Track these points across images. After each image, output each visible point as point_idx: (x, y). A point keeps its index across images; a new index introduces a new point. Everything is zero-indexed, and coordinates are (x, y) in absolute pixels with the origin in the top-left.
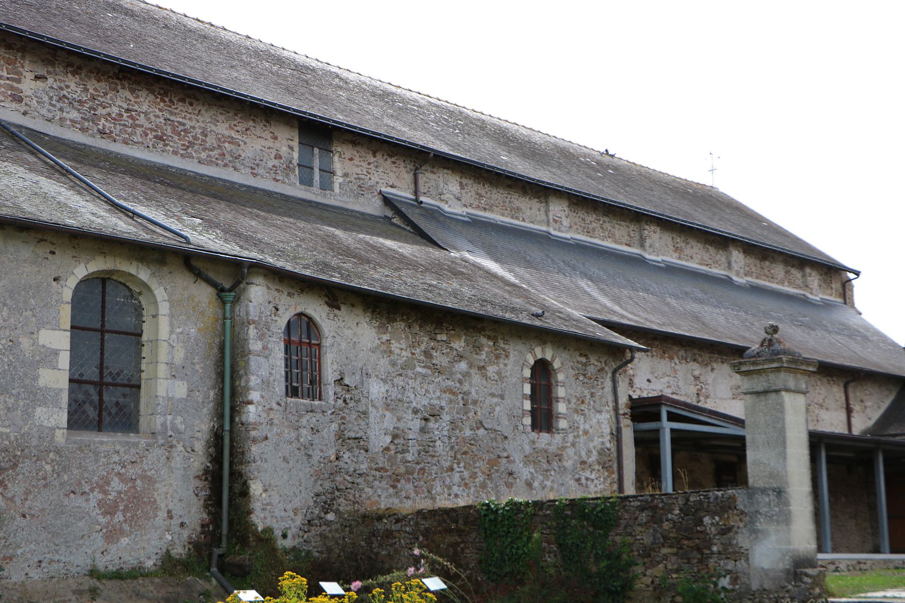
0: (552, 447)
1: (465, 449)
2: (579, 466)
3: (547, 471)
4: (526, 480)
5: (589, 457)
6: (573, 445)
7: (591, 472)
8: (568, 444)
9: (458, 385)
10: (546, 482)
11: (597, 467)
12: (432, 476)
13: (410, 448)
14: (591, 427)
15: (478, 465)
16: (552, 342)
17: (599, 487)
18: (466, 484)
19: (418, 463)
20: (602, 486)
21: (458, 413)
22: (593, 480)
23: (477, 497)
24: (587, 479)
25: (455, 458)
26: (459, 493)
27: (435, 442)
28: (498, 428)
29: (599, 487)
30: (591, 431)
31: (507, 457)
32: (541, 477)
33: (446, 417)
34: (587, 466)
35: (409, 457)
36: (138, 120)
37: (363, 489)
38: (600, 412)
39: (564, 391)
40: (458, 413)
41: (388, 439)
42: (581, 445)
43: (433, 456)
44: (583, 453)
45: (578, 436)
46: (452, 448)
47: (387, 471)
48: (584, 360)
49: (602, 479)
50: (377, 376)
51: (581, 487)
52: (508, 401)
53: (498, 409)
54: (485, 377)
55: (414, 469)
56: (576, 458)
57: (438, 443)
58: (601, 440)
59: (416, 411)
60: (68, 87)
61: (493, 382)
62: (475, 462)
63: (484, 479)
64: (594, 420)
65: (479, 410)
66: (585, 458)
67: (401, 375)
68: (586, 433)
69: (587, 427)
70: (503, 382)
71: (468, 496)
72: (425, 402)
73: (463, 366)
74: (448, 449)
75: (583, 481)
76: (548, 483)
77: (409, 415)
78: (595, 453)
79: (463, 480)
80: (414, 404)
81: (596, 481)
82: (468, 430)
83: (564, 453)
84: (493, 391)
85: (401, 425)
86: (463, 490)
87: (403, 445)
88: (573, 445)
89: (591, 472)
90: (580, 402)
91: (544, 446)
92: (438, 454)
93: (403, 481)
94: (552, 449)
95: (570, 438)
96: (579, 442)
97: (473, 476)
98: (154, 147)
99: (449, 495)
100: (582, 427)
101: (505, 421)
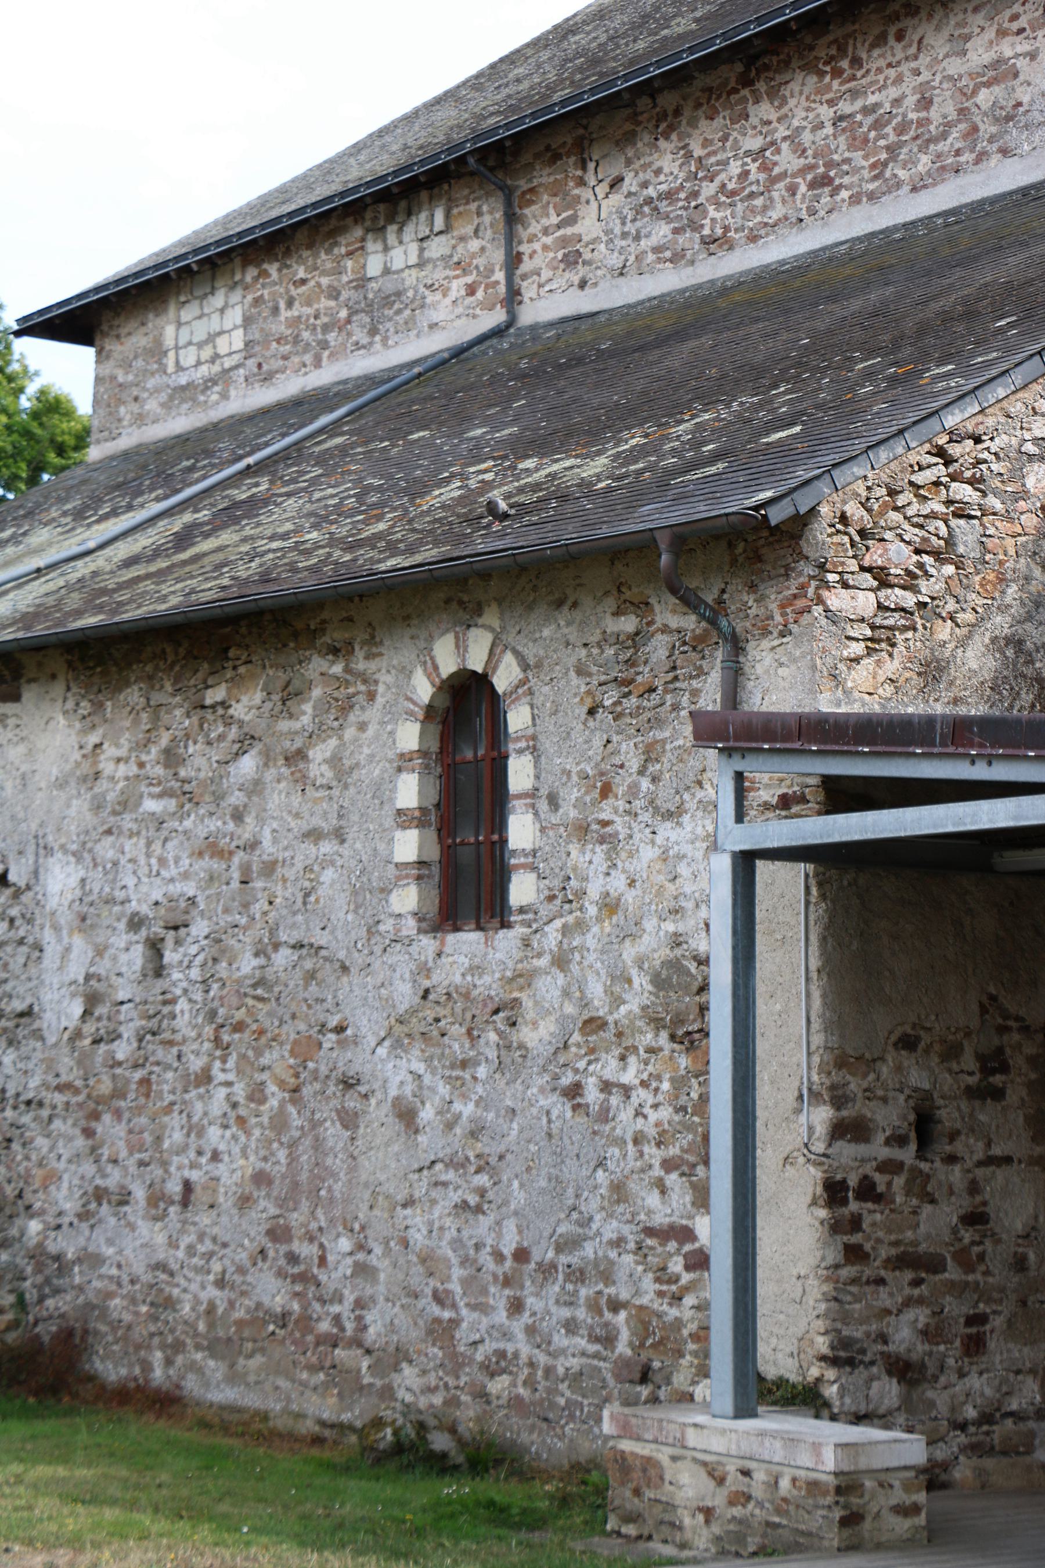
0: (487, 979)
1: (240, 1015)
2: (576, 1037)
3: (464, 1064)
4: (397, 1099)
5: (617, 1001)
6: (561, 962)
7: (623, 1058)
8: (543, 962)
9: (231, 826)
10: (457, 1107)
11: (648, 1038)
12: (162, 1099)
13: (122, 1029)
14: (632, 883)
15: (265, 1060)
16: (500, 601)
17: (653, 1116)
18: (241, 1121)
19: (136, 1066)
20: (665, 1113)
21: (226, 911)
22: (626, 1091)
23: (265, 1159)
24: (606, 1087)
25: (217, 1040)
26: (222, 1147)
27: (173, 1001)
28: (321, 938)
29: (653, 1116)
30: (630, 897)
31: (340, 1029)
32: (444, 1090)
33: (200, 928)
34: (609, 1034)
35: (123, 1050)
36: (775, 164)
37: (32, 1141)
38: (673, 815)
39: (530, 769)
40: (226, 911)
41: (77, 1009)
42: (591, 957)
43: (171, 1043)
44: (596, 990)
45: (581, 926)
46: (212, 1014)
47: (77, 1091)
48: (628, 624)
49: (666, 1086)
50: (62, 847)
51: (582, 1120)
52: (357, 844)
53: (328, 875)
54: (302, 781)
55: (128, 1081)
56: (569, 1009)
57: (182, 1005)
58: (670, 927)
59: (136, 923)
60: (658, 172)
61: (322, 793)
62: (259, 1053)
63: (282, 1103)
64: (648, 853)
65: (279, 890)
66: (600, 1006)
67: (109, 832)
68: (610, 906)
69: (618, 883)
70: (346, 787)
71: (244, 1155)
72: (157, 895)
73: (248, 764)
74: (200, 1020)
75: (592, 1095)
76: (467, 1109)
77: (121, 939)
78: (641, 981)
79: (235, 1105)
80: (134, 903)
81: (641, 1095)
82: (248, 955)
83: (523, 996)
84: (317, 822)
85: (102, 967)
86: (234, 1137)
87: (109, 1019)
88: (561, 962)
89: (623, 1058)
90: (596, 794)
91: (458, 979)
92: (178, 1037)
93: (107, 1118)
94: (488, 985)
95: (552, 935)
96: (582, 949)
97: (257, 1095)
98: (812, 212)
99: (200, 1153)
100: (594, 890)
101: (341, 913)
